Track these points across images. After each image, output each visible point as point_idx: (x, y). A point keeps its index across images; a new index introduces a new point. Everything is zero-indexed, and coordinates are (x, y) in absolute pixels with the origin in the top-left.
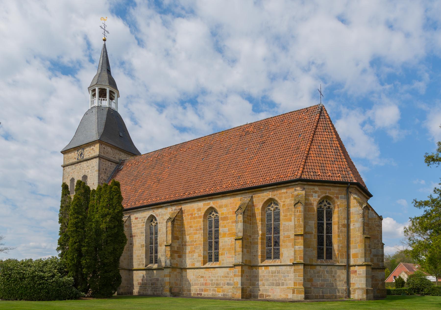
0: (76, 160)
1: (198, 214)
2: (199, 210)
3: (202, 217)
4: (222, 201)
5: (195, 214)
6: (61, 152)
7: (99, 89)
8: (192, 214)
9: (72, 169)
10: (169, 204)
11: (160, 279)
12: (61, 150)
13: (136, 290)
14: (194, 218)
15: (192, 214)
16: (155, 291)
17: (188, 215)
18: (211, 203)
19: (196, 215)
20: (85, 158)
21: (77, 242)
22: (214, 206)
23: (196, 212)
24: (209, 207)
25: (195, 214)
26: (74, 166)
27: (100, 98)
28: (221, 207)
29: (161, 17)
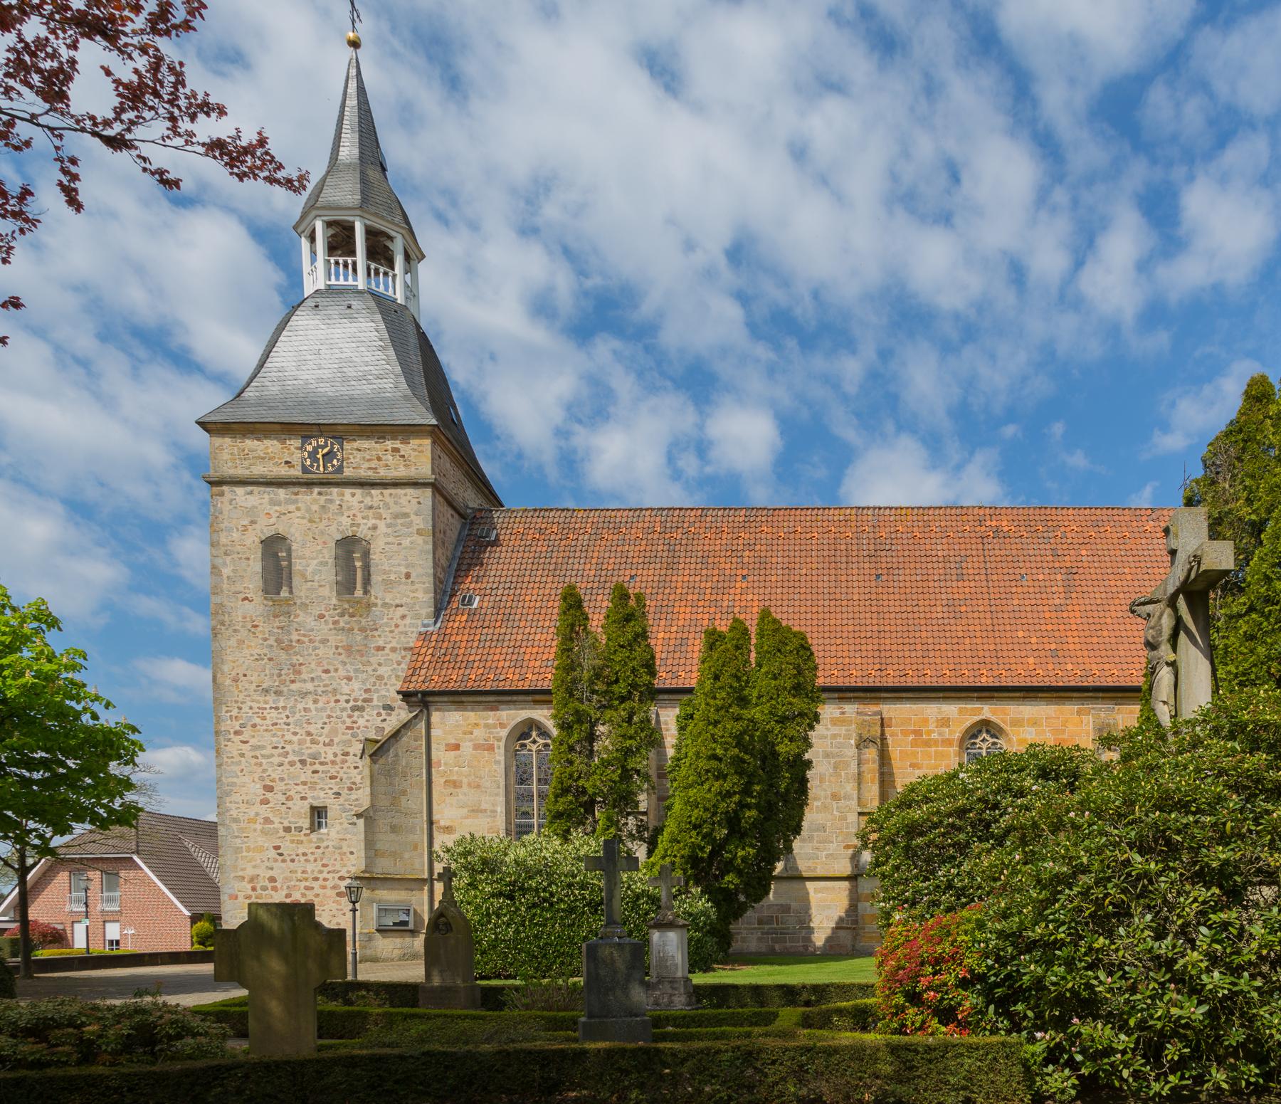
0: (296, 472)
1: (940, 734)
2: (944, 722)
3: (956, 743)
4: (1021, 708)
5: (929, 732)
6: (202, 424)
7: (329, 224)
8: (918, 733)
9: (273, 503)
10: (836, 695)
11: (794, 905)
12: (200, 413)
13: (819, 939)
14: (927, 744)
15: (918, 733)
16: (775, 941)
17: (905, 733)
18: (987, 711)
19: (935, 736)
20: (348, 472)
21: (735, 793)
22: (993, 719)
23: (932, 726)
24: (976, 718)
25: (929, 732)
26: (282, 493)
27: (332, 260)
28: (1017, 723)
29: (1224, 180)
